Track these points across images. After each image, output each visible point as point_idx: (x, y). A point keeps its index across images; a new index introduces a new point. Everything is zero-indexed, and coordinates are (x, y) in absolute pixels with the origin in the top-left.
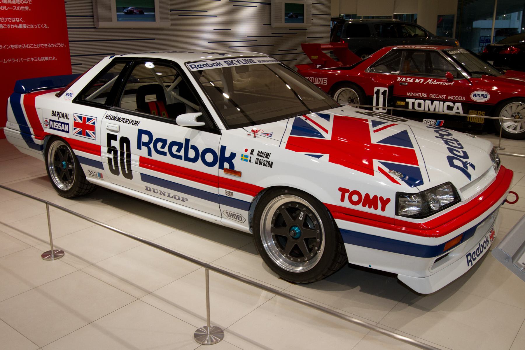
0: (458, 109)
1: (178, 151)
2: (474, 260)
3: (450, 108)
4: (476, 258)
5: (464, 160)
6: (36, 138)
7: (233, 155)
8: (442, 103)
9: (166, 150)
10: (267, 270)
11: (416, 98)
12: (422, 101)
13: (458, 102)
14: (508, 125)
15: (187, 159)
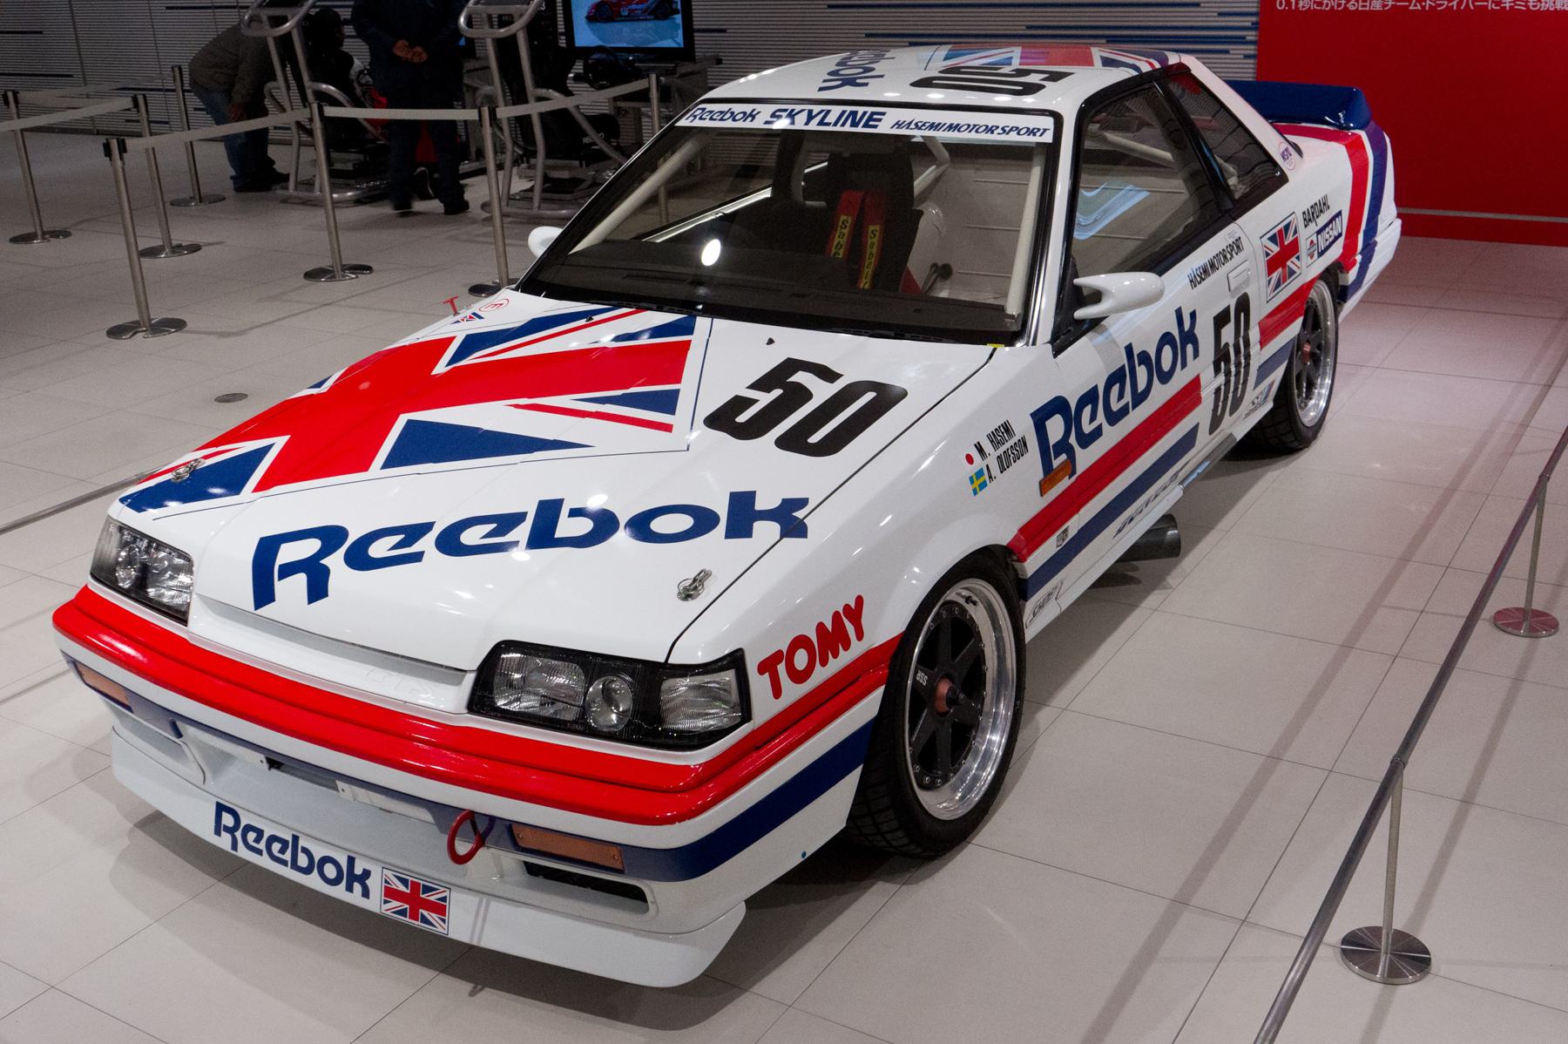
1: (282, 851)
2: (1086, 440)
4: (1097, 433)
5: (1072, 440)
6: (409, 422)
7: (367, 874)
9: (262, 846)
15: (295, 866)
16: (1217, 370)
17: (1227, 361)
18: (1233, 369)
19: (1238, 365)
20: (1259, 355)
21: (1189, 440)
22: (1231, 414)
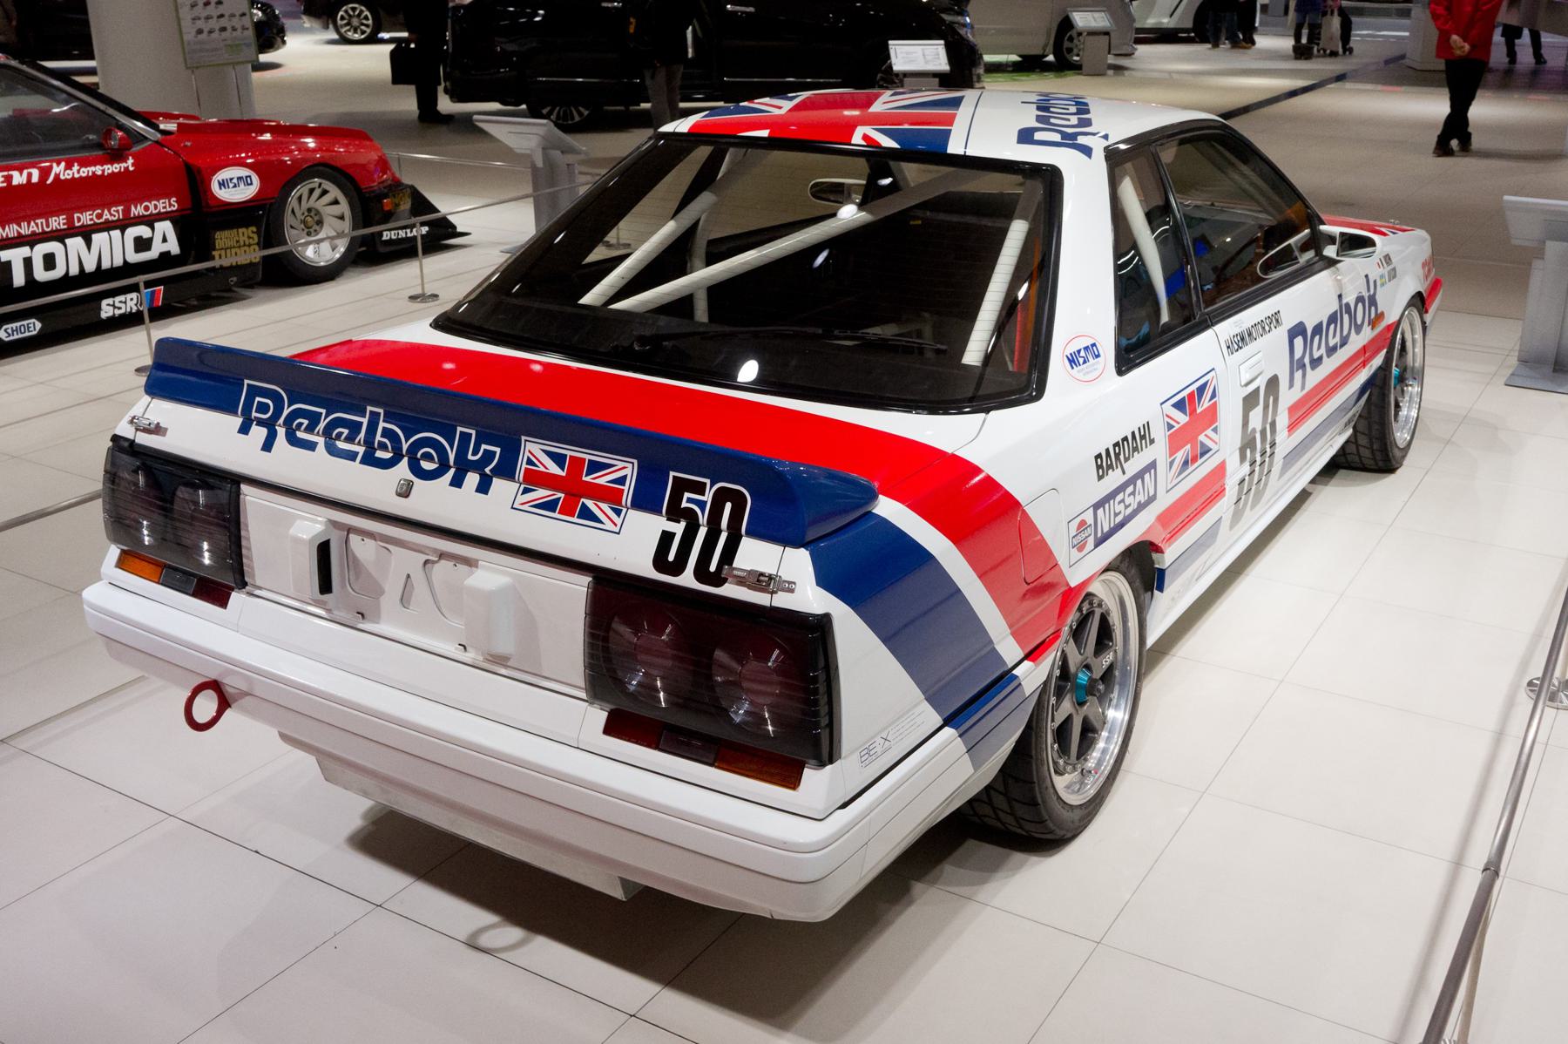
0: (165, 240)
3: (142, 244)
5: (1307, 360)
8: (116, 234)
10: (1377, 480)
11: (32, 241)
12: (53, 247)
13: (161, 217)
14: (319, 251)
16: (1243, 458)
17: (1253, 450)
18: (1258, 459)
19: (1263, 453)
20: (1285, 442)
21: (1211, 534)
22: (1253, 507)
